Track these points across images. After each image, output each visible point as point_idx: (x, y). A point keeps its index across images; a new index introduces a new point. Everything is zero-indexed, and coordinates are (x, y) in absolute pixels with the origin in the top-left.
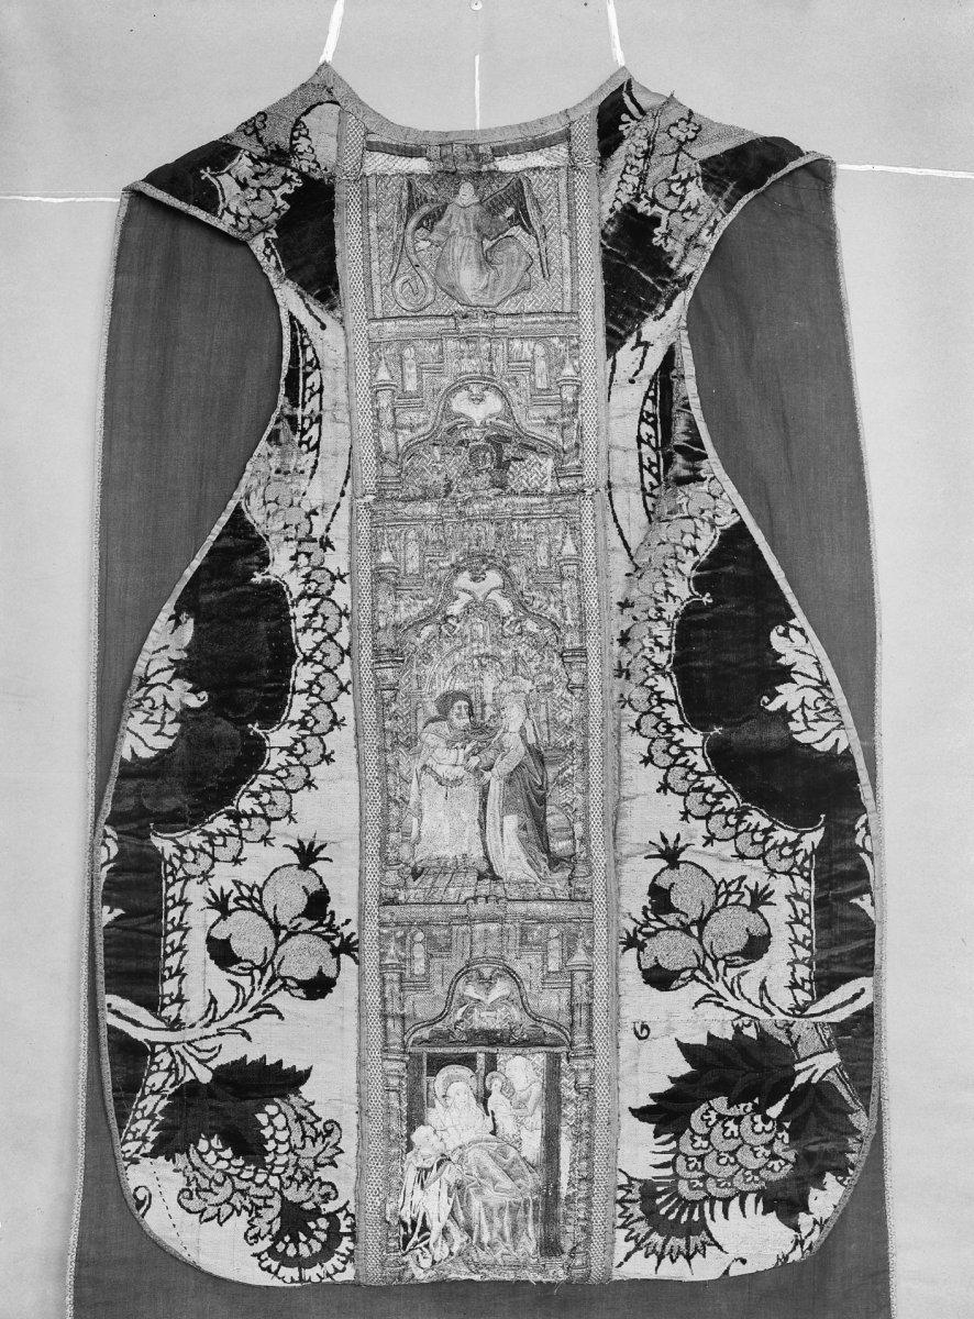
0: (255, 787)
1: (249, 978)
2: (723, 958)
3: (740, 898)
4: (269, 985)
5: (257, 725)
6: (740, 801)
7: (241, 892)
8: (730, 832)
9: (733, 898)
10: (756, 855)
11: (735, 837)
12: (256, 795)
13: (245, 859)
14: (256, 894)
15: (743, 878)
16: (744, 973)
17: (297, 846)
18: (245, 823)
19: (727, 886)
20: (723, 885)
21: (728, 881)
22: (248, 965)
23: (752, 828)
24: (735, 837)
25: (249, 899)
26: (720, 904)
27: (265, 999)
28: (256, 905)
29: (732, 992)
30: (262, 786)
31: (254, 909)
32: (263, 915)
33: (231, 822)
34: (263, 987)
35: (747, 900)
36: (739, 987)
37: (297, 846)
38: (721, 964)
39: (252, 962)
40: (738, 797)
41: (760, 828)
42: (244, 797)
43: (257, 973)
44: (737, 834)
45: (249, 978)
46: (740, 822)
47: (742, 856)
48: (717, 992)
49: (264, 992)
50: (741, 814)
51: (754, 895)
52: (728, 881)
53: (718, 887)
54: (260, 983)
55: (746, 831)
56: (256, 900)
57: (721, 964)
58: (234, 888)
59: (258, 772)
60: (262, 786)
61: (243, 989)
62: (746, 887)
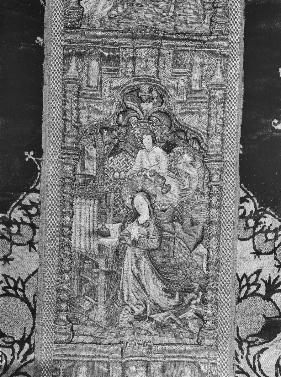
0: (25, 202)
1: (11, 350)
2: (246, 341)
3: (258, 288)
4: (25, 356)
5: (32, 153)
6: (258, 205)
7: (8, 283)
8: (250, 232)
9: (253, 288)
10: (269, 251)
11: (253, 237)
12: (26, 208)
13: (13, 259)
14: (20, 286)
15: (258, 272)
16: (262, 351)
17: (32, 249)
18: (14, 229)
19: (10, 287)
20: (244, 279)
21: (24, 279)
22: (10, 340)
23: (266, 228)
24: (253, 237)
25: (15, 288)
26: (242, 296)
27: (22, 366)
28: (20, 293)
29: (254, 369)
30: (31, 202)
31: (17, 296)
32: (25, 299)
33: (4, 227)
34: (21, 357)
35: (262, 291)
36: (260, 366)
37: (32, 249)
38: (245, 345)
39: (13, 338)
40: (256, 201)
41: (272, 228)
42: (16, 209)
43: (17, 347)
44: (255, 234)
45: (11, 350)
46: (257, 224)
47: (258, 253)
48: (242, 370)
49: (22, 361)
50: (256, 216)
51: (267, 284)
52: (24, 279)
53: (240, 281)
54: (19, 353)
55: (261, 231)
56: (20, 290)
57: (245, 345)
58: (3, 279)
59: (29, 192)
60: (31, 202)
61: (6, 357)
62: (261, 279)
